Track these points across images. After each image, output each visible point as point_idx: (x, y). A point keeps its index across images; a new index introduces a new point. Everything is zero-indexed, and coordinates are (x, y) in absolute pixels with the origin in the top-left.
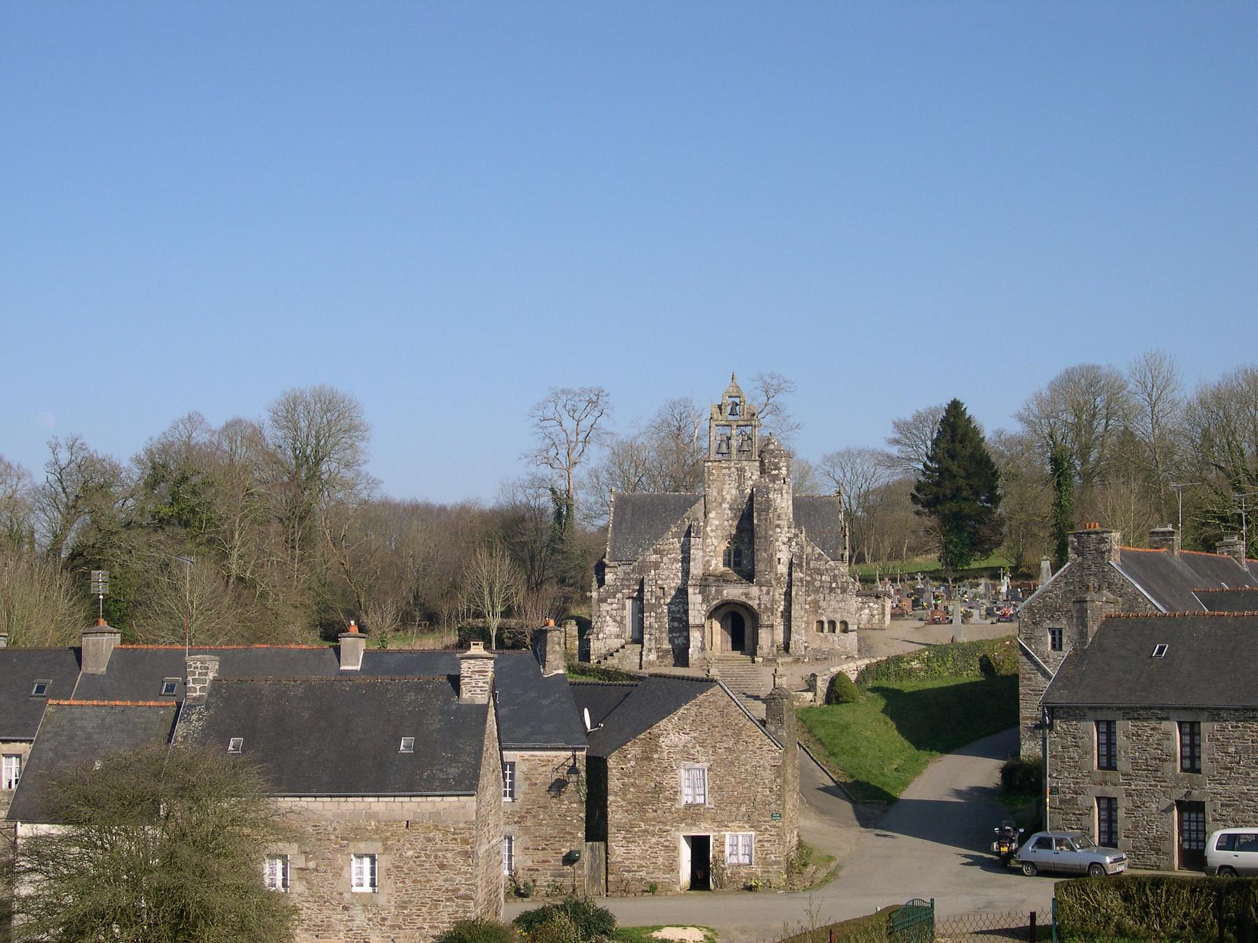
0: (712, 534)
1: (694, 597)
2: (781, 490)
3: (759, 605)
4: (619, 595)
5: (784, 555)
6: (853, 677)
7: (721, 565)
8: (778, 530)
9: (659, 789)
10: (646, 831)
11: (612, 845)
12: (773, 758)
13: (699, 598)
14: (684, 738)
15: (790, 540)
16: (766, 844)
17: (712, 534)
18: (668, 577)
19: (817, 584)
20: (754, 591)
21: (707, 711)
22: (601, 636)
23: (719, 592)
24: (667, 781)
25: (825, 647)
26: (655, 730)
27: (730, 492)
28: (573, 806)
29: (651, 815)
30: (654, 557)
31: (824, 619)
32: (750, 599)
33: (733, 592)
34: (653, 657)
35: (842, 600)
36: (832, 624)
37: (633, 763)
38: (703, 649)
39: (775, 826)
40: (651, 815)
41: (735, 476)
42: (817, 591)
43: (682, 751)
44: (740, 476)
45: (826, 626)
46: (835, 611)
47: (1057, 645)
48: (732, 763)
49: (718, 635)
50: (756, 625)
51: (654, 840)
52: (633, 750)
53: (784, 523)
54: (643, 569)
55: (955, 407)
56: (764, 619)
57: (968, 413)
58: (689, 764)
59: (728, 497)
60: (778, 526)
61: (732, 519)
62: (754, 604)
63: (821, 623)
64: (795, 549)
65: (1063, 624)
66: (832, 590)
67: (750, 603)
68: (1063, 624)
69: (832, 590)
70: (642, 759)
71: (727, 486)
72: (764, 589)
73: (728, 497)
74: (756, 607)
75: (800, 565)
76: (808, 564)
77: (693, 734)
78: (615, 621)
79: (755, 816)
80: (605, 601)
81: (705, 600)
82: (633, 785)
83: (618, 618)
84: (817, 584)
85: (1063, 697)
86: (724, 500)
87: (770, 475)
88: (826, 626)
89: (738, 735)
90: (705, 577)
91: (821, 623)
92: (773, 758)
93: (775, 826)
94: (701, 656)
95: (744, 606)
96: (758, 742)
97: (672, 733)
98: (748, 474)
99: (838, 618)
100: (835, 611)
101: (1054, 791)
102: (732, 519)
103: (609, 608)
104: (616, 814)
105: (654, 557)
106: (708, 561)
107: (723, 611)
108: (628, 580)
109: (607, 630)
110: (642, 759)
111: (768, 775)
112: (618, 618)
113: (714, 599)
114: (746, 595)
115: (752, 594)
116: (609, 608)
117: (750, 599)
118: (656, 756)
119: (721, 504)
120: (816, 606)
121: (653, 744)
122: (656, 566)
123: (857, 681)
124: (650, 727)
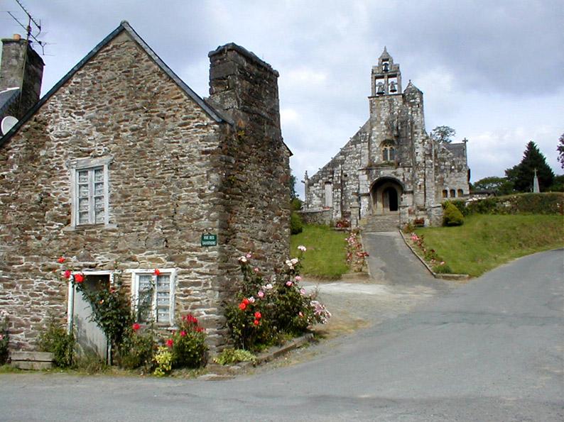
0: (375, 141)
2: (417, 111)
3: (404, 179)
4: (321, 181)
7: (381, 160)
8: (416, 135)
9: (45, 202)
10: (27, 269)
12: (204, 139)
13: (366, 177)
14: (79, 120)
15: (423, 141)
16: (194, 290)
17: (375, 141)
18: (349, 168)
19: (443, 167)
20: (400, 170)
21: (108, 75)
22: (310, 206)
23: (378, 173)
24: (56, 191)
29: (33, 244)
31: (448, 189)
32: (398, 175)
35: (459, 176)
37: (16, 167)
39: (205, 258)
40: (33, 244)
41: (387, 105)
42: (442, 171)
43: (73, 143)
44: (390, 104)
45: (449, 193)
46: (454, 183)
48: (141, 152)
51: (36, 283)
55: (531, 145)
57: (537, 148)
59: (384, 118)
60: (416, 133)
61: (387, 130)
62: (400, 178)
63: (445, 192)
64: (427, 146)
66: (452, 170)
67: (398, 178)
69: (452, 170)
70: (26, 160)
71: (382, 111)
72: (406, 169)
73: (384, 118)
74: (401, 180)
75: (430, 155)
76: (436, 156)
77: (89, 113)
78: (318, 196)
79: (176, 241)
80: (313, 185)
81: (370, 177)
82: (15, 199)
83: (320, 195)
84: (443, 167)
86: (381, 119)
87: (409, 103)
88: (449, 193)
89: (149, 107)
91: (445, 192)
92: (204, 139)
93: (205, 258)
94: (368, 213)
96: (181, 116)
98: (395, 103)
99: (456, 188)
100: (454, 183)
102: (387, 130)
103: (315, 189)
106: (373, 157)
107: (384, 186)
108: (325, 172)
109: (314, 202)
110: (26, 160)
112: (320, 195)
113: (375, 177)
114: (395, 173)
115: (401, 174)
116: (315, 189)
117: (398, 175)
118: (42, 153)
119: (379, 122)
120: (442, 181)
124: (36, 112)
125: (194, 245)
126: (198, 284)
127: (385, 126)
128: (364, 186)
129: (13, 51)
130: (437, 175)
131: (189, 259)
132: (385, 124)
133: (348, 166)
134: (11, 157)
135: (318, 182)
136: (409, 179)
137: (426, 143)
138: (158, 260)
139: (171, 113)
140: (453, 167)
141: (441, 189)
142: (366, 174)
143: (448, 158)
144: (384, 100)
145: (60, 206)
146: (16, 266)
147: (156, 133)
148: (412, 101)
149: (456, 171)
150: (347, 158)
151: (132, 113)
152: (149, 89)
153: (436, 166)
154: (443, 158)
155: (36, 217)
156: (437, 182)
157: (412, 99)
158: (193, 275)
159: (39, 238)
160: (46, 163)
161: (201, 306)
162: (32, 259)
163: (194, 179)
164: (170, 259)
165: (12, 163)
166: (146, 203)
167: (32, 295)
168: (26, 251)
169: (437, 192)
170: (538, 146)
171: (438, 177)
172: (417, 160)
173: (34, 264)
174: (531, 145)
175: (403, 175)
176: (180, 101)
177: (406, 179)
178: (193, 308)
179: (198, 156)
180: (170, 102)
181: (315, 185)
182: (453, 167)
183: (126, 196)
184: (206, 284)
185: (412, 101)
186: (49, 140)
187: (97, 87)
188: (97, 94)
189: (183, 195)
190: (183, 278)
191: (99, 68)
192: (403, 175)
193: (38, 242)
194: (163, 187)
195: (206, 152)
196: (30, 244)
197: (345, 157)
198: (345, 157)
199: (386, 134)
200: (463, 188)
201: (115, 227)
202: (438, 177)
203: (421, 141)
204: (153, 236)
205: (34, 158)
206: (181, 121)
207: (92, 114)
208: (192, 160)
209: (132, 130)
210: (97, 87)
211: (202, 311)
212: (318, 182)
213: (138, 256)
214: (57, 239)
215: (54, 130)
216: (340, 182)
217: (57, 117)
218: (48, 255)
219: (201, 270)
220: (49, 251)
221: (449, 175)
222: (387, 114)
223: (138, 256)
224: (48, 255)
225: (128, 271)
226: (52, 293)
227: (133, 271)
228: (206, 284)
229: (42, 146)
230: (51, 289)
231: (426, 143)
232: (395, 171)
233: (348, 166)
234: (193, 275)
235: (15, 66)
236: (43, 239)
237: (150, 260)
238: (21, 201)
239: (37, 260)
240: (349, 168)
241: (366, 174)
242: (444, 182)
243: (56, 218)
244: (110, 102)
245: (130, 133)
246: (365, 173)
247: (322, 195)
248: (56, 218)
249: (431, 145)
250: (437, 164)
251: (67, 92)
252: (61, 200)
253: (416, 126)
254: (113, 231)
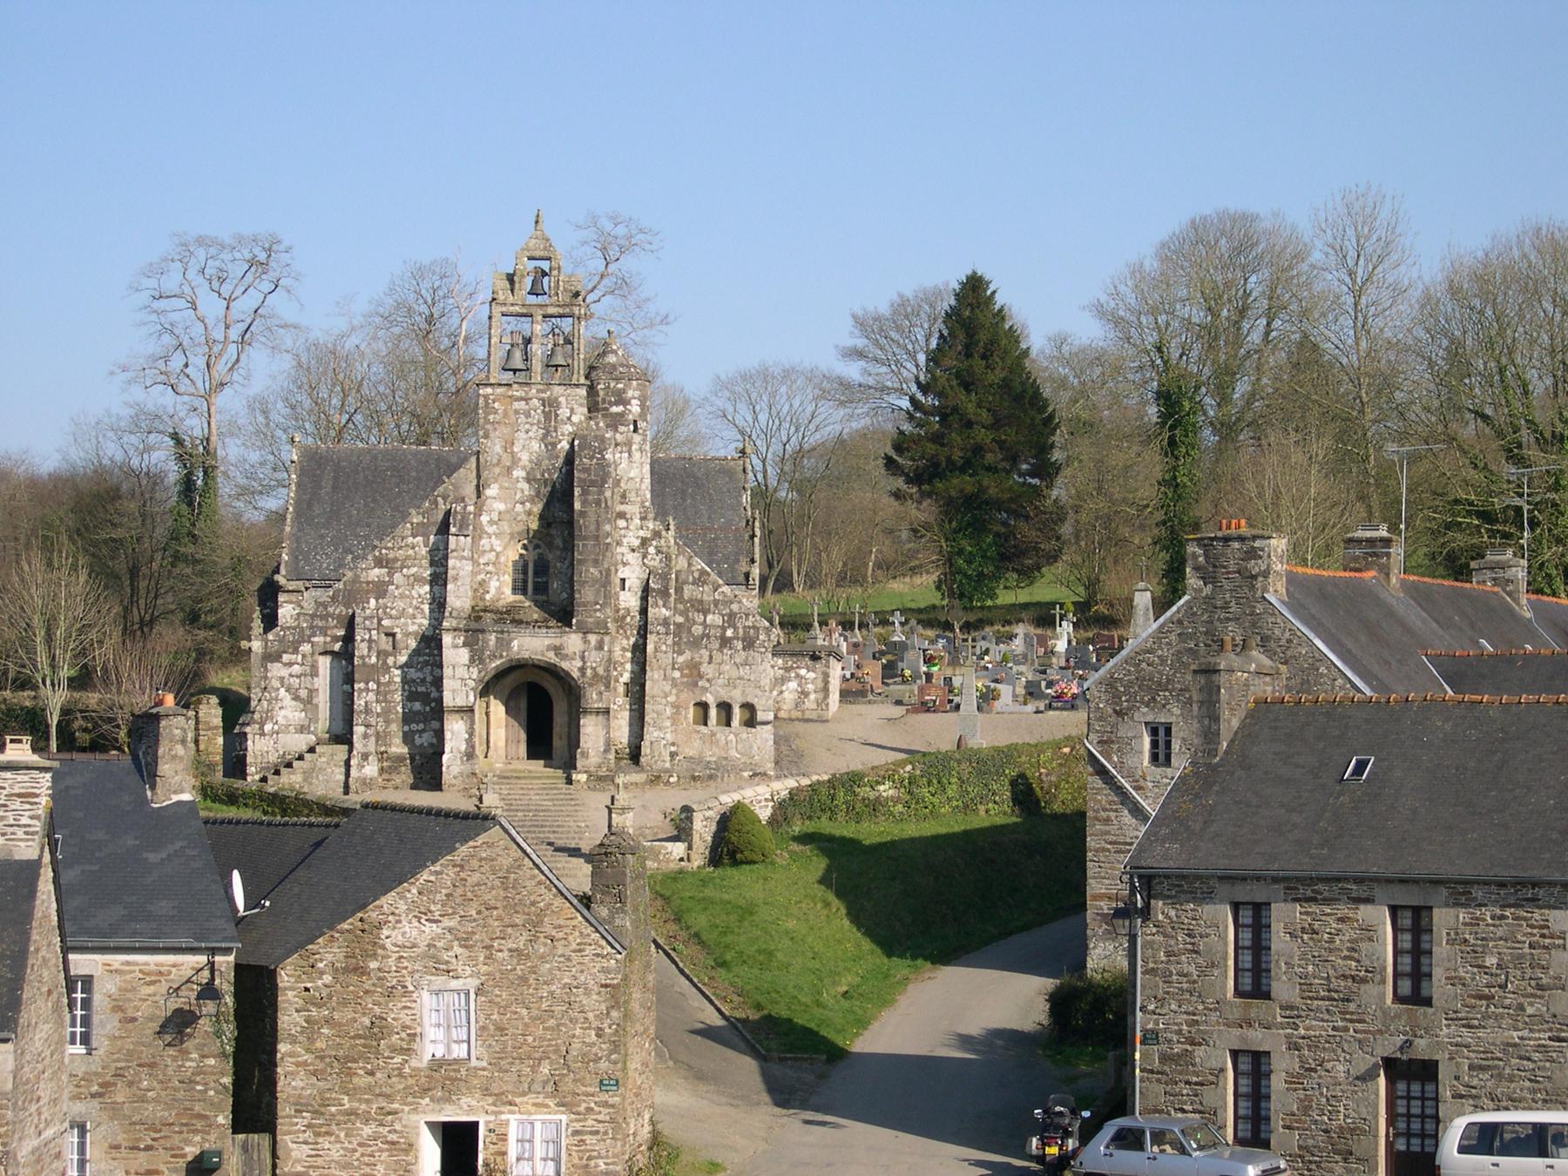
0: (491, 529)
1: (455, 654)
2: (629, 444)
3: (582, 670)
4: (306, 648)
5: (632, 573)
6: (764, 813)
7: (508, 591)
8: (622, 523)
9: (378, 1029)
10: (352, 1113)
11: (285, 1139)
13: (464, 655)
14: (430, 929)
15: (645, 542)
17: (491, 529)
18: (402, 613)
19: (697, 630)
21: (476, 878)
22: (268, 728)
23: (504, 644)
24: (396, 1014)
25: (710, 755)
26: (372, 914)
27: (528, 447)
28: (208, 1063)
29: (362, 1080)
30: (376, 573)
31: (710, 699)
32: (565, 657)
33: (532, 644)
34: (371, 770)
36: (725, 708)
37: (327, 979)
38: (470, 755)
39: (606, 1104)
41: (538, 415)
42: (696, 643)
43: (424, 956)
44: (547, 416)
46: (731, 683)
47: (1161, 756)
48: (524, 980)
49: (501, 728)
50: (576, 709)
51: (367, 1130)
52: (329, 952)
53: (632, 509)
54: (354, 595)
56: (592, 698)
57: (1000, 300)
58: (439, 981)
59: (525, 457)
60: (622, 515)
61: (532, 500)
62: (572, 667)
64: (655, 561)
65: (1173, 714)
66: (725, 642)
67: (565, 665)
68: (1173, 714)
69: (725, 642)
70: (346, 970)
71: (522, 435)
72: (593, 638)
73: (525, 457)
74: (575, 674)
76: (679, 590)
77: (447, 923)
78: (296, 698)
79: (568, 1085)
81: (476, 658)
82: (328, 1021)
83: (303, 693)
84: (697, 630)
85: (1170, 856)
86: (515, 461)
88: (713, 712)
90: (476, 614)
91: (703, 706)
92: (605, 970)
93: (606, 1104)
94: (467, 768)
95: (552, 671)
97: (405, 921)
98: (564, 412)
99: (736, 697)
100: (731, 683)
101: (1151, 1037)
103: (284, 672)
104: (293, 1078)
105: (376, 573)
107: (510, 681)
108: (322, 618)
109: (281, 716)
110: (346, 970)
111: (594, 1003)
112: (303, 693)
113: (493, 657)
114: (557, 649)
115: (569, 650)
117: (565, 657)
118: (373, 965)
119: (509, 470)
121: (367, 943)
122: (380, 590)
123: (773, 821)
125: (590, 1090)
126: (597, 1132)
127: (526, 486)
128: (457, 684)
129: (177, 732)
130: (680, 653)
131: (584, 1105)
132: (528, 480)
133: (400, 604)
134: (321, 965)
135: (296, 651)
136: (601, 671)
137: (652, 550)
138: (547, 1106)
139: (561, 935)
140: (729, 633)
141: (689, 699)
142: (465, 645)
143: (716, 603)
144: (527, 400)
145: (404, 1035)
146: (333, 1109)
147: (542, 957)
148: (615, 409)
149: (739, 645)
150: (398, 577)
151: (509, 930)
152: (533, 904)
153: (678, 625)
154: (701, 602)
155: (364, 1046)
156: (677, 674)
157: (617, 404)
158: (590, 1122)
159: (371, 1073)
160: (379, 979)
161: (599, 1157)
162: (360, 1100)
163: (591, 1015)
164: (558, 1105)
165: (322, 973)
166: (530, 1039)
167: (360, 1145)
168: (351, 1092)
169: (676, 707)
170: (1008, 294)
171: (681, 659)
172: (623, 605)
173: (363, 1106)
174: (974, 289)
175: (583, 658)
176: (574, 923)
177: (589, 672)
178: (589, 1159)
179: (596, 988)
180: (562, 922)
181: (286, 658)
182: (729, 633)
183: (503, 1029)
184: (606, 1133)
185: (615, 409)
186: (384, 948)
187: (460, 891)
188: (458, 900)
189: (578, 1032)
190: (578, 1126)
191: (462, 867)
192: (583, 658)
193: (370, 1079)
194: (552, 1022)
195: (606, 986)
196: (355, 1080)
197: (390, 574)
198: (390, 574)
199: (529, 513)
200: (755, 701)
201: (484, 1064)
202: (681, 659)
203: (637, 543)
204: (540, 1078)
205: (361, 971)
206: (574, 946)
207: (452, 924)
208: (587, 992)
209: (510, 950)
210: (460, 891)
211: (601, 1162)
212: (296, 651)
213: (518, 1100)
214: (400, 1075)
215: (391, 937)
216: (374, 660)
217: (399, 922)
218: (388, 1096)
219: (600, 1117)
220: (388, 1091)
221: (717, 656)
222: (535, 446)
223: (518, 1100)
224: (388, 1096)
225: (503, 1117)
226: (393, 1143)
227: (511, 1117)
228: (606, 1133)
229: (374, 956)
230: (394, 1137)
231: (652, 550)
232: (557, 642)
233: (400, 604)
234: (590, 1122)
235: (181, 758)
236: (379, 1075)
237: (534, 1105)
238: (340, 1024)
239: (368, 1101)
240: (402, 613)
241: (465, 645)
242: (701, 677)
243: (395, 1050)
244: (479, 913)
245: (506, 954)
246: (461, 641)
247: (311, 691)
248: (395, 1050)
249: (668, 557)
250: (680, 619)
251: (415, 891)
252: (405, 1027)
253: (624, 496)
254: (484, 1069)
